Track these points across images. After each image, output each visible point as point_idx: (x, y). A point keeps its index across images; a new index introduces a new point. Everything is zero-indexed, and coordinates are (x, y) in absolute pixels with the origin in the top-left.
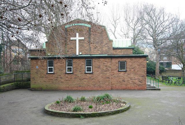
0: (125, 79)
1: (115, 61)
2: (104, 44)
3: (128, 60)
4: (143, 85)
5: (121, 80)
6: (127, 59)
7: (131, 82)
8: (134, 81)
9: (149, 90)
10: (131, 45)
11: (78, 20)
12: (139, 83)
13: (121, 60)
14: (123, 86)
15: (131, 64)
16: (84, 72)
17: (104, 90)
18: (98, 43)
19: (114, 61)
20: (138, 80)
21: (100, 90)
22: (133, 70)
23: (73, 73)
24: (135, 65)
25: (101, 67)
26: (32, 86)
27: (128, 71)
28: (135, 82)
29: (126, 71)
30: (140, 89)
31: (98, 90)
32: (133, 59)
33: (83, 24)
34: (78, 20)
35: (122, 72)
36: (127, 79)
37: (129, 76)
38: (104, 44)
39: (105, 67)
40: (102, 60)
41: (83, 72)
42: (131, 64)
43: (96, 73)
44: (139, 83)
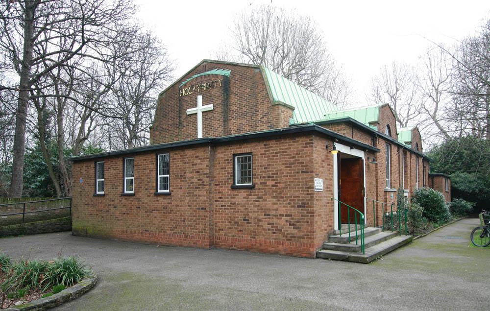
0: (251, 214)
1: (223, 154)
2: (259, 117)
3: (257, 149)
4: (303, 238)
5: (240, 216)
6: (253, 145)
7: (266, 226)
8: (275, 220)
9: (327, 257)
10: (364, 119)
11: (205, 63)
12: (292, 230)
13: (239, 151)
14: (245, 237)
15: (264, 161)
16: (153, 191)
17: (193, 247)
18: (245, 114)
19: (222, 155)
20: (288, 218)
21: (186, 245)
22: (271, 183)
23: (133, 195)
24: (279, 165)
25: (188, 175)
26: (76, 225)
27: (257, 187)
28: (280, 227)
29: (251, 188)
30: (295, 252)
31: (181, 246)
32: (272, 143)
33: (214, 72)
34: (205, 63)
35: (243, 191)
36: (256, 215)
37: (261, 203)
38: (259, 117)
39: (196, 175)
40: (189, 153)
41: (151, 191)
42: (264, 161)
43: (178, 194)
44: (292, 230)
